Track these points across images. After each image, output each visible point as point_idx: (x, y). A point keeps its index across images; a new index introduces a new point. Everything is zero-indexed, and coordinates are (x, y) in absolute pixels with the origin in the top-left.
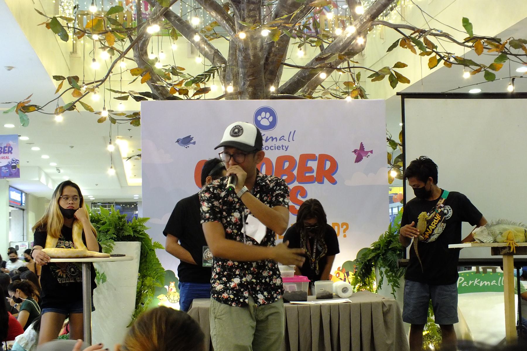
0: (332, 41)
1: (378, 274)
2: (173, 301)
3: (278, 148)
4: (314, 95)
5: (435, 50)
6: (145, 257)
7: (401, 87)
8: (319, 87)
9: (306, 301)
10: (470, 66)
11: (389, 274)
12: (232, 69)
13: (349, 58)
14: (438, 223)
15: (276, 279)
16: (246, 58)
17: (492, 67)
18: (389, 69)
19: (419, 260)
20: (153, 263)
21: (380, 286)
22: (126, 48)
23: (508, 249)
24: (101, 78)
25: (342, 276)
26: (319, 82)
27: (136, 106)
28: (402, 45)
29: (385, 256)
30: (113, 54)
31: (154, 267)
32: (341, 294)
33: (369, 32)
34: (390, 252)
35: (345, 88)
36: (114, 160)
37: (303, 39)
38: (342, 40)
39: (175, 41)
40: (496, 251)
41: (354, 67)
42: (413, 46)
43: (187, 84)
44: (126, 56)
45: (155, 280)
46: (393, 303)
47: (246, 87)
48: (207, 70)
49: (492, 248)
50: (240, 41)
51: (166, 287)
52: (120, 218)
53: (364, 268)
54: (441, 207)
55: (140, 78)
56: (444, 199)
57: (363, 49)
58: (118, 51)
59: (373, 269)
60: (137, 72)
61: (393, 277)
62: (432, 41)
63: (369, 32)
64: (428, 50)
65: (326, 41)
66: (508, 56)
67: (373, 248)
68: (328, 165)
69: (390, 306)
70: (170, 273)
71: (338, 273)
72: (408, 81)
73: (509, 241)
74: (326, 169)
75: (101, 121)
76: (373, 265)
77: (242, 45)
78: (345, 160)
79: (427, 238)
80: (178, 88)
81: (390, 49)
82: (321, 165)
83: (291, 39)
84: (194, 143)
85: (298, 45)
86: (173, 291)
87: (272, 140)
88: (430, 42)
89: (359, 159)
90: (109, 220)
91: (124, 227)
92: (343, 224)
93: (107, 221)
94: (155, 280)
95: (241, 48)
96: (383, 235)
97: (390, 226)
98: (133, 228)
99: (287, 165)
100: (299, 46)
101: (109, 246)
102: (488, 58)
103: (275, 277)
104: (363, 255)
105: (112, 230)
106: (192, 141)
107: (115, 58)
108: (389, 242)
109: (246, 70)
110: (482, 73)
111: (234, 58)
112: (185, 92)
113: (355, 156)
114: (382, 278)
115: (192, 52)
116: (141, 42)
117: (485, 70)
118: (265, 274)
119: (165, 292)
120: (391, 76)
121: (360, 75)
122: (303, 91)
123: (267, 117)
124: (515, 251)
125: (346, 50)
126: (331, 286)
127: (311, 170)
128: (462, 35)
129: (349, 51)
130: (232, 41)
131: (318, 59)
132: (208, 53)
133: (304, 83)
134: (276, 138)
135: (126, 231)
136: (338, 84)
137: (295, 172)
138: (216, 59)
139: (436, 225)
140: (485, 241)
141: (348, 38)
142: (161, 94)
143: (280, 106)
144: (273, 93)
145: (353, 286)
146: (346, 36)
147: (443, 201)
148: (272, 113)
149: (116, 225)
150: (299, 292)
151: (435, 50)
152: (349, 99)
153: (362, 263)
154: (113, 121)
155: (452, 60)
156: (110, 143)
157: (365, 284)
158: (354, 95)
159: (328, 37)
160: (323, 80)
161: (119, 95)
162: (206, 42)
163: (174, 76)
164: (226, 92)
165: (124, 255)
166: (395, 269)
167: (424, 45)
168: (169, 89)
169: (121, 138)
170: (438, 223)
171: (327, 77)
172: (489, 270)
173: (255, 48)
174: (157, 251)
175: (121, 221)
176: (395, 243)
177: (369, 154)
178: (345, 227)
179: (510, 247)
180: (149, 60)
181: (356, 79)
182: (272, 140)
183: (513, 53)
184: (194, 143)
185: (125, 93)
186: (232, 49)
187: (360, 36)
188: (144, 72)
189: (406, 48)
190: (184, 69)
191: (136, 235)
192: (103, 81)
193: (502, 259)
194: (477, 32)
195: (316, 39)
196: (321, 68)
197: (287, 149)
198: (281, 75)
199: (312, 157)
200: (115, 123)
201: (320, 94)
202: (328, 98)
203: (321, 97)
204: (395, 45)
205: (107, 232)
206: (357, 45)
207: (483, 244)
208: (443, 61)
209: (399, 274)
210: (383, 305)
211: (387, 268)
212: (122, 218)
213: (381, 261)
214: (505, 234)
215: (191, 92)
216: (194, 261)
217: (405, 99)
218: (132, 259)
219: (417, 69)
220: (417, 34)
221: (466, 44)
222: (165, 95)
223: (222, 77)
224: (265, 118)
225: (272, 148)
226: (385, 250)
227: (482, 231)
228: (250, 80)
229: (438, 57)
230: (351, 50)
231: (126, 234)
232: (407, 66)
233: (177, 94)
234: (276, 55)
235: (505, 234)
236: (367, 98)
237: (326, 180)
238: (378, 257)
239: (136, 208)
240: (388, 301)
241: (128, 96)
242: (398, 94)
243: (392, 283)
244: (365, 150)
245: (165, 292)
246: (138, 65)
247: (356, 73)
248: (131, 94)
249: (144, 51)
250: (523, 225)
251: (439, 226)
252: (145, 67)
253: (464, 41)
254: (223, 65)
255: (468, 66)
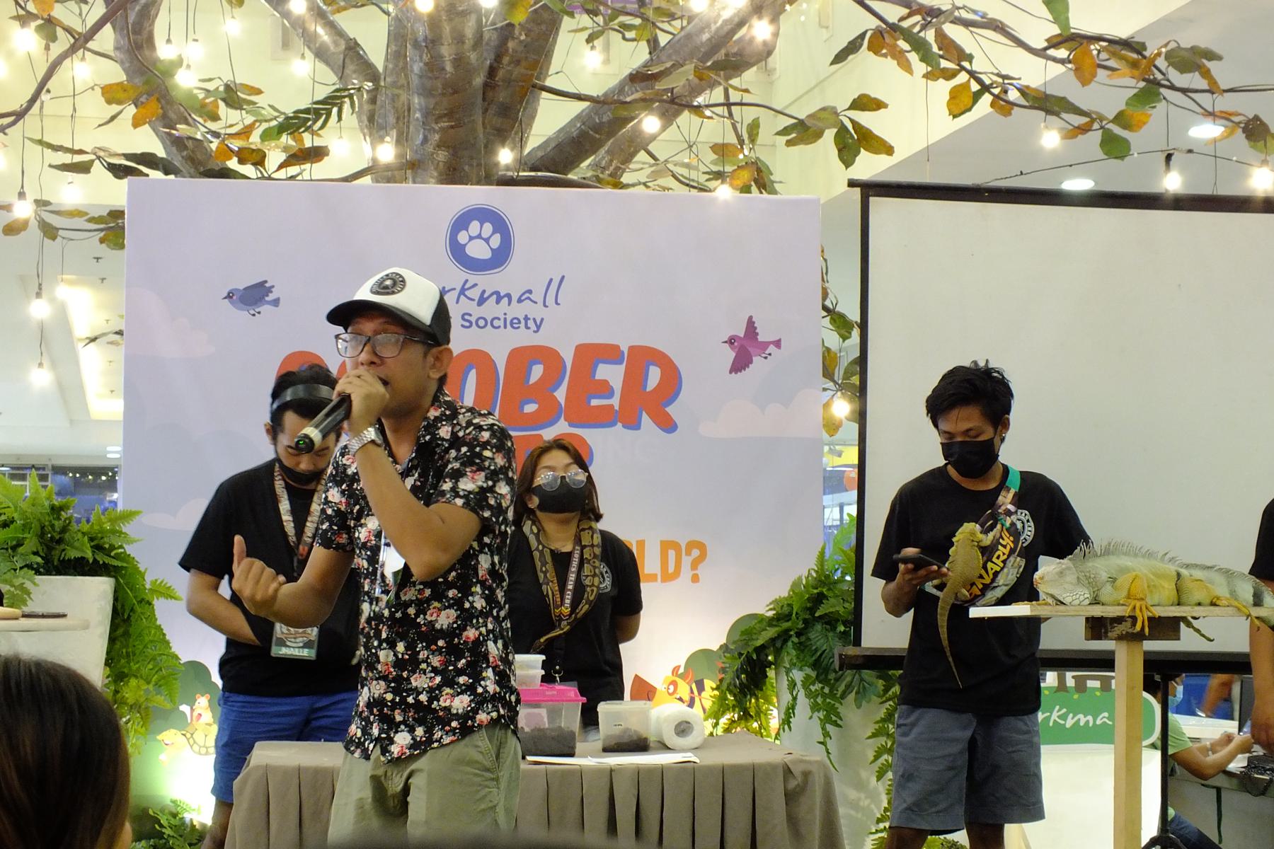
0: (682, 28)
1: (786, 685)
2: (203, 751)
3: (515, 323)
4: (625, 179)
5: (966, 64)
6: (124, 621)
7: (869, 166)
8: (642, 156)
9: (572, 755)
10: (1064, 115)
11: (813, 688)
12: (394, 98)
13: (727, 78)
14: (1009, 556)
15: (453, 696)
16: (434, 66)
17: (1120, 119)
18: (837, 114)
19: (948, 654)
20: (147, 639)
21: (786, 721)
22: (91, 20)
23: (1129, 624)
24: (15, 106)
25: (684, 690)
26: (640, 143)
27: (115, 193)
28: (875, 48)
29: (803, 639)
30: (54, 38)
31: (150, 651)
32: (671, 739)
33: (788, 7)
34: (818, 627)
35: (714, 163)
36: (51, 342)
37: (600, 19)
38: (708, 26)
39: (237, 11)
40: (1097, 627)
41: (741, 104)
42: (903, 52)
43: (266, 136)
44: (90, 45)
45: (151, 687)
46: (814, 769)
47: (430, 148)
48: (320, 96)
49: (1087, 619)
50: (418, 17)
51: (185, 708)
52: (56, 510)
53: (746, 670)
54: (1008, 513)
55: (131, 110)
56: (1013, 491)
57: (769, 53)
58: (68, 30)
59: (771, 673)
60: (121, 95)
61: (824, 696)
62: (959, 42)
63: (788, 7)
64: (944, 64)
65: (666, 26)
66: (1162, 90)
67: (771, 614)
68: (654, 376)
69: (806, 774)
70: (198, 669)
71: (674, 683)
72: (889, 150)
73: (1133, 603)
74: (649, 388)
75: (12, 229)
76: (770, 664)
77: (421, 31)
78: (704, 362)
79: (977, 596)
80: (235, 145)
81: (840, 58)
82: (634, 379)
83: (566, 19)
84: (276, 302)
85: (585, 35)
86: (203, 720)
87: (498, 302)
88: (953, 41)
89: (740, 364)
90: (23, 513)
91: (67, 536)
92: (692, 545)
93: (16, 516)
94: (151, 687)
95: (421, 38)
96: (800, 578)
97: (822, 553)
98: (91, 539)
99: (537, 372)
100: (590, 40)
101: (21, 587)
102: (1109, 93)
103: (448, 690)
104: (743, 633)
105: (31, 543)
106: (271, 297)
107: (57, 49)
108: (818, 599)
109: (432, 102)
110: (1095, 137)
111: (401, 64)
112: (256, 157)
113: (730, 355)
114: (795, 699)
115: (286, 45)
116: (138, 8)
117: (1102, 127)
118: (419, 681)
119: (182, 723)
120: (842, 130)
121: (758, 126)
122: (596, 166)
123: (485, 235)
124: (1147, 630)
125: (720, 55)
126: (645, 715)
127: (604, 389)
128: (1040, 30)
129: (725, 58)
130: (397, 19)
131: (638, 78)
132: (328, 49)
133: (598, 142)
134: (509, 296)
135: (73, 547)
136: (694, 149)
137: (561, 394)
138: (350, 67)
139: (1004, 562)
140: (1067, 600)
141: (725, 22)
142: (191, 160)
143: (520, 205)
144: (508, 168)
145: (711, 721)
146: (719, 16)
147: (1010, 495)
148: (501, 225)
149: (43, 528)
150: (552, 730)
151: (966, 64)
152: (724, 192)
153: (740, 654)
154: (50, 232)
155: (1013, 95)
156: (38, 295)
157: (746, 716)
158: (739, 183)
159: (672, 17)
160: (653, 138)
161: (67, 158)
162: (321, 15)
163: (231, 111)
164: (374, 160)
165: (64, 616)
166: (832, 676)
167: (935, 49)
168: (214, 146)
169: (71, 283)
170: (1009, 556)
171: (664, 128)
172: (1090, 684)
173: (459, 39)
174: (160, 605)
175: (59, 519)
176: (832, 600)
177: (772, 349)
178: (696, 553)
179: (1134, 619)
180: (156, 61)
181: (745, 136)
182: (498, 302)
183: (1178, 84)
184: (276, 302)
185: (81, 152)
186: (396, 39)
187: (760, 18)
188: (140, 95)
189: (885, 56)
190: (259, 92)
191: (101, 560)
192: (20, 115)
193: (1113, 653)
194: (1081, 22)
195: (638, 21)
196: (646, 103)
197: (538, 327)
198: (533, 117)
199: (609, 353)
200: (54, 238)
201: (642, 176)
202: (664, 189)
203: (644, 184)
204: (852, 47)
205: (14, 548)
206: (752, 40)
207: (1062, 608)
208: (987, 98)
209: (842, 688)
210: (788, 771)
211: (808, 671)
212: (61, 508)
213: (794, 653)
214: (1124, 581)
215: (275, 157)
216: (254, 638)
217: (872, 199)
218: (86, 627)
219: (916, 118)
220: (918, 18)
221: (1051, 52)
222: (200, 163)
223: (365, 118)
224: (479, 236)
225: (496, 323)
226: (805, 621)
227: (1061, 574)
228: (442, 129)
229: (975, 87)
230: (735, 54)
231: (72, 554)
232: (885, 106)
233: (233, 164)
234: (518, 62)
235: (1124, 581)
236: (774, 192)
237: (646, 419)
238: (785, 641)
239: (112, 485)
240: (802, 761)
241: (93, 161)
242: (852, 184)
243: (822, 714)
244: (760, 338)
245: (182, 723)
246: (127, 74)
247: (748, 120)
248: (99, 158)
249: (145, 36)
250: (1171, 560)
251: (1009, 564)
252: (147, 83)
253: (1046, 44)
254: (368, 85)
255: (1057, 114)
